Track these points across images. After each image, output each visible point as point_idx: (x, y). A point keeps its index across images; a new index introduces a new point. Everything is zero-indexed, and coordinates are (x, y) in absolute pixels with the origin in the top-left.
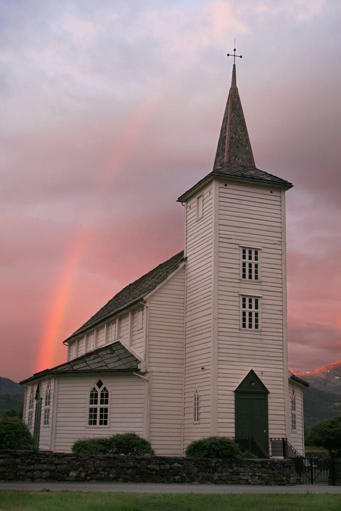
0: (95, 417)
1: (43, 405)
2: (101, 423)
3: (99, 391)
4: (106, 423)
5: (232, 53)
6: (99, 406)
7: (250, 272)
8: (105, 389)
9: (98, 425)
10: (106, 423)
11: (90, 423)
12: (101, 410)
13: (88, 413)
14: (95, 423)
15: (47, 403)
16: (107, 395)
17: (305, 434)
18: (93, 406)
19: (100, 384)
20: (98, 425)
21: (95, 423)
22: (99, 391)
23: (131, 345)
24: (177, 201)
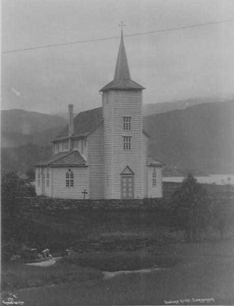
0: (68, 183)
1: (46, 178)
2: (71, 186)
3: (70, 173)
4: (73, 186)
5: (121, 24)
6: (70, 179)
7: (126, 138)
8: (72, 172)
9: (70, 187)
10: (73, 186)
11: (153, 185)
12: (71, 180)
13: (65, 182)
14: (68, 186)
15: (48, 177)
16: (73, 175)
17: (204, 184)
18: (68, 179)
19: (70, 170)
20: (70, 187)
21: (68, 186)
22: (70, 173)
23: (82, 153)
24: (144, 89)
